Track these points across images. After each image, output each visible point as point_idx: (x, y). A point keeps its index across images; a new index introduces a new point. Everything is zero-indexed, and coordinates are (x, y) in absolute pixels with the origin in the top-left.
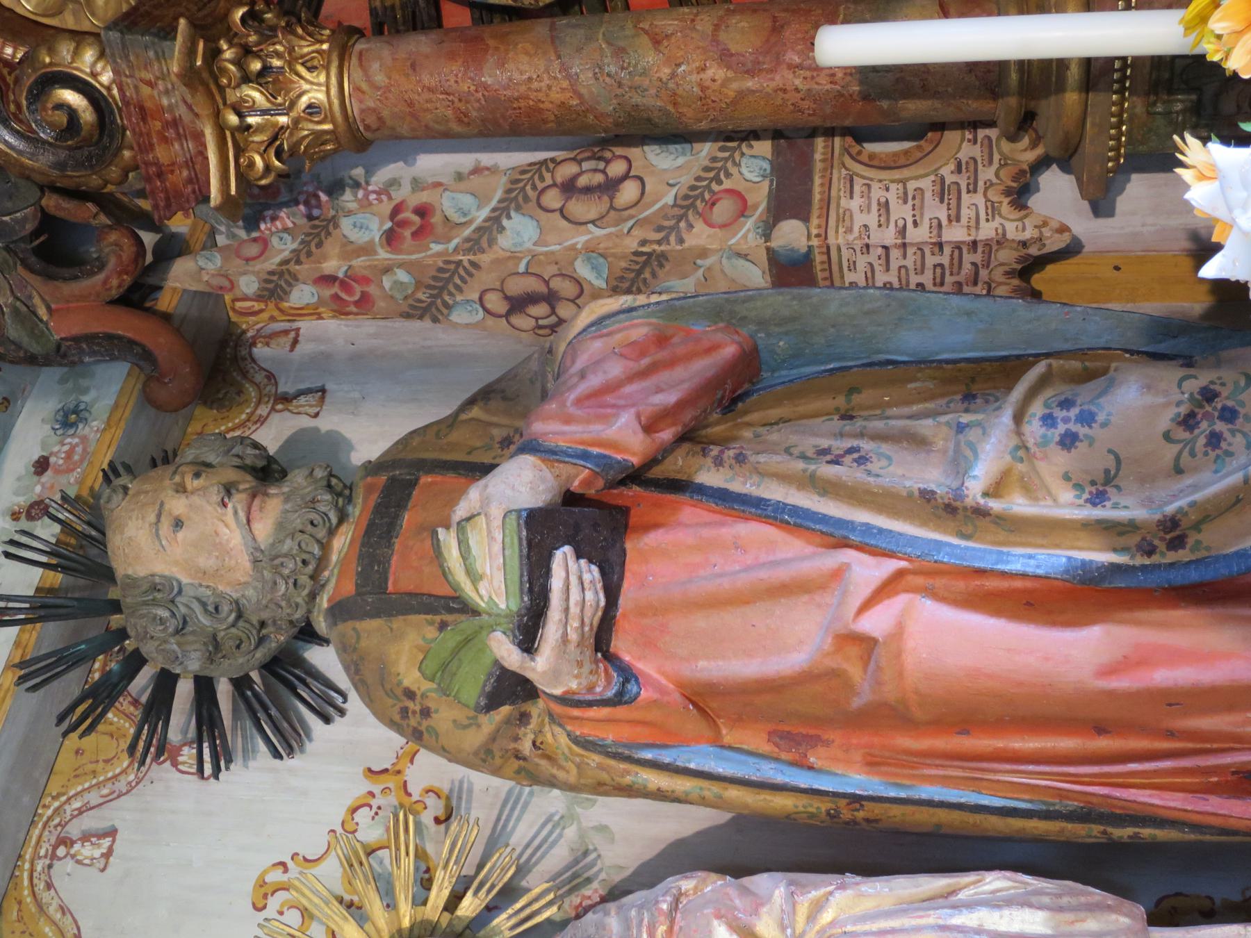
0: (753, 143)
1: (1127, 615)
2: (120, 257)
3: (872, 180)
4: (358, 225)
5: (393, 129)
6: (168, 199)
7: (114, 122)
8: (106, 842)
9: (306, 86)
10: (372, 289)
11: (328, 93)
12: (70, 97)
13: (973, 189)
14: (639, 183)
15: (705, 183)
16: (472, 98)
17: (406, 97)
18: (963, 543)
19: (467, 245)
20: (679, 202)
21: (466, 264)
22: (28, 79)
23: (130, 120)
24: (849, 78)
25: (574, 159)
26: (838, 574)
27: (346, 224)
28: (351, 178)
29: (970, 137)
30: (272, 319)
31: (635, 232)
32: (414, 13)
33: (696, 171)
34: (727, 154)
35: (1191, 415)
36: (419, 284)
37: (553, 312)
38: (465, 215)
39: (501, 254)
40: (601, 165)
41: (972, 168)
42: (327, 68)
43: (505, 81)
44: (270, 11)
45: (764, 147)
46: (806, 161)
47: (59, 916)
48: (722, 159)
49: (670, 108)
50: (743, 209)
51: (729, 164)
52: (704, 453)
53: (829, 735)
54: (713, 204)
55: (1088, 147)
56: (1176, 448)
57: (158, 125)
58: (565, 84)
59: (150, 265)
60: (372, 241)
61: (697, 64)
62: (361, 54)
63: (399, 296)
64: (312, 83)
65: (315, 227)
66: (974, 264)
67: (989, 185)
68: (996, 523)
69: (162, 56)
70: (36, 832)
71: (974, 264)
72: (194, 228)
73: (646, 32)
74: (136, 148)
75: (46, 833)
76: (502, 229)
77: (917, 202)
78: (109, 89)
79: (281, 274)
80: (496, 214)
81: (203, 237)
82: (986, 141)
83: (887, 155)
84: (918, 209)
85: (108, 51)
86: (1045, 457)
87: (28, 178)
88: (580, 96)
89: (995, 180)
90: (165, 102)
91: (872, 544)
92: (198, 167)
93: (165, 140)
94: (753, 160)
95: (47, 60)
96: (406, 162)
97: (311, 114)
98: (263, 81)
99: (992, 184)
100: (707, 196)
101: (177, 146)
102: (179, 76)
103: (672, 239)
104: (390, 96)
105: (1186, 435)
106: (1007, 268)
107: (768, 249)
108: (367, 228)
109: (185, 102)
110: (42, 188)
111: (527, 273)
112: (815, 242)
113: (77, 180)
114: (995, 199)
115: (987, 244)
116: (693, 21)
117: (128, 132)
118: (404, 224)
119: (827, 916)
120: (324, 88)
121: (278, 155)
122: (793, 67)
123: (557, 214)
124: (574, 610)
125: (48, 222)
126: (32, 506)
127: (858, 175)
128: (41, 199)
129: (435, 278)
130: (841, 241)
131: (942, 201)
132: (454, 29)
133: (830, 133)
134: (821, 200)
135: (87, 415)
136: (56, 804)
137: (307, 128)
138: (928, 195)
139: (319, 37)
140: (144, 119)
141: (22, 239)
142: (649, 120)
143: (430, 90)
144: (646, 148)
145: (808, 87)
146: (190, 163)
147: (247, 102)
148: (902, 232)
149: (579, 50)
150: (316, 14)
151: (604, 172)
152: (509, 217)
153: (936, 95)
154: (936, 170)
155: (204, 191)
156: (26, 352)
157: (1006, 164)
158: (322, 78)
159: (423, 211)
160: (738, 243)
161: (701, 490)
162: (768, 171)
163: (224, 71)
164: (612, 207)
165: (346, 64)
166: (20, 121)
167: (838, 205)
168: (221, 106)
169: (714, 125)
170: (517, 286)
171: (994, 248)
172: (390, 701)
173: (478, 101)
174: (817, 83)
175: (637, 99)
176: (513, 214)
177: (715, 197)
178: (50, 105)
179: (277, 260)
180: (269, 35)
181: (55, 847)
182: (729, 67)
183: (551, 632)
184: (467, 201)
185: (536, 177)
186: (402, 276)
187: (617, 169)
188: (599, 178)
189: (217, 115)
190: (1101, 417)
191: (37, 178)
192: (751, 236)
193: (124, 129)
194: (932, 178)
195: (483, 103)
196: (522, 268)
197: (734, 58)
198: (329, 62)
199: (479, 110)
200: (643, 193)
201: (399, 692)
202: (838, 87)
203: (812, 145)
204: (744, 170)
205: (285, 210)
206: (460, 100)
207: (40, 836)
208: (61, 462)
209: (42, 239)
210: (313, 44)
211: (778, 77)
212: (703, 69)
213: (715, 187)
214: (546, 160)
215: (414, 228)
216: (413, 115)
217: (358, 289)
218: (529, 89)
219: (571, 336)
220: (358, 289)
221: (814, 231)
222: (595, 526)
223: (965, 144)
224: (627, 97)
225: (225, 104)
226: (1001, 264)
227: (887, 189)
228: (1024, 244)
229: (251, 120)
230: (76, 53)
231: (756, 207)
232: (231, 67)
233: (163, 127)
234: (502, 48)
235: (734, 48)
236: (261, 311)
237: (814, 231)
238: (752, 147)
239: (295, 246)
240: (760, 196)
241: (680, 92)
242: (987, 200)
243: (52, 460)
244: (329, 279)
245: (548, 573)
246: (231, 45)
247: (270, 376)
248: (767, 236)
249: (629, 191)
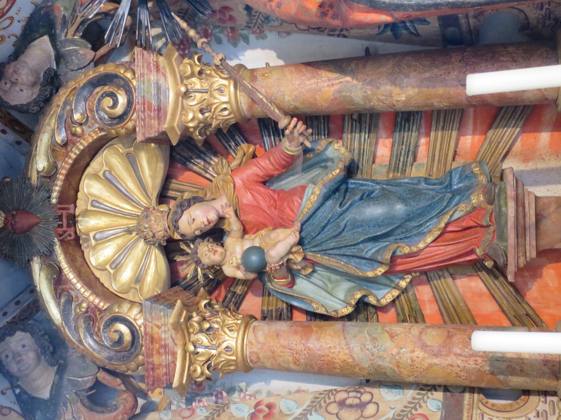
0: (434, 392)
2: (125, 406)
3: (493, 416)
4: (239, 408)
5: (263, 363)
6: (154, 381)
7: (138, 342)
9: (227, 338)
11: (236, 342)
12: (123, 328)
14: (376, 406)
15: (409, 409)
16: (302, 353)
17: (272, 349)
20: (396, 417)
23: (146, 342)
24: (484, 363)
25: (346, 391)
27: (233, 408)
28: (239, 387)
29: (543, 400)
32: (281, 314)
33: (405, 403)
34: (420, 397)
38: (290, 411)
40: (359, 395)
41: (545, 415)
42: (238, 331)
43: (318, 347)
44: (217, 304)
45: (439, 395)
46: (459, 404)
48: (418, 399)
49: (396, 369)
51: (421, 402)
57: (157, 346)
58: (347, 351)
59: (138, 414)
61: (411, 349)
62: (254, 327)
65: (218, 407)
69: (166, 316)
72: (162, 400)
73: (387, 332)
74: (145, 355)
78: (140, 327)
80: (305, 412)
81: (165, 405)
82: (551, 403)
83: (501, 405)
85: (144, 310)
87: (94, 362)
88: (353, 358)
90: (163, 336)
92: (171, 368)
93: (159, 353)
94: (433, 401)
95: (117, 310)
96: (266, 383)
97: (227, 351)
98: (208, 333)
100: (409, 416)
101: (164, 357)
102: (172, 324)
104: (265, 347)
108: (243, 411)
109: (172, 337)
110: (99, 368)
113: (115, 366)
116: (410, 329)
117: (143, 348)
118: (260, 411)
120: (235, 340)
121: (208, 368)
122: (457, 355)
123: (335, 415)
125: (97, 384)
127: (486, 413)
128: (97, 373)
132: (298, 322)
133: (472, 390)
137: (224, 357)
139: (237, 317)
140: (152, 342)
141: (83, 390)
142: (385, 373)
143: (284, 347)
144: (381, 389)
145: (463, 365)
146: (168, 366)
147: (200, 341)
149: (355, 336)
150: (238, 309)
151: (359, 398)
152: (311, 414)
153: (527, 375)
154: (526, 415)
155: (171, 381)
158: (235, 335)
159: (270, 406)
162: (441, 407)
163: (192, 326)
164: (362, 416)
165: (247, 331)
166: (98, 336)
168: (187, 342)
169: (416, 379)
173: (305, 355)
174: (469, 364)
175: (380, 363)
176: (313, 413)
177: (414, 417)
178: (113, 330)
180: (215, 313)
182: (426, 352)
184: (292, 404)
185: (327, 397)
187: (366, 398)
188: (357, 401)
189: (185, 345)
191: (98, 363)
193: (142, 346)
195: (307, 356)
197: (428, 348)
198: (239, 329)
199: (305, 359)
200: (378, 411)
202: (478, 367)
203: (463, 396)
204: (428, 405)
205: (206, 398)
206: (297, 353)
209: (93, 392)
210: (234, 320)
211: (449, 359)
212: (413, 352)
213: (414, 412)
214: (332, 390)
215: (265, 414)
216: (273, 358)
218: (330, 352)
223: (541, 403)
224: (375, 361)
225: (189, 341)
229: (200, 350)
230: (130, 309)
232: (196, 325)
233: (159, 347)
234: (319, 332)
235: (429, 343)
238: (433, 394)
239: (207, 414)
241: (401, 361)
246: (198, 315)
249: (371, 409)
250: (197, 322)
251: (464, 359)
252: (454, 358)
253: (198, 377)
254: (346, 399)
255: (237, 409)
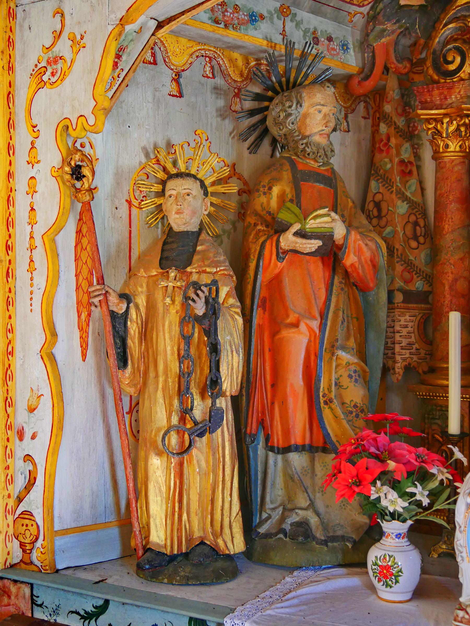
1: (306, 391)
8: (211, 75)
10: (384, 154)
12: (458, 60)
13: (411, 353)
18: (324, 350)
19: (398, 190)
20: (410, 261)
21: (392, 189)
22: (464, 47)
26: (314, 318)
30: (372, 108)
31: (401, 247)
33: (420, 266)
34: (424, 276)
35: (357, 407)
36: (386, 171)
37: (374, 217)
39: (395, 202)
47: (189, 62)
49: (441, 262)
50: (407, 282)
51: (421, 277)
52: (343, 279)
53: (267, 314)
54: (409, 272)
55: (423, 387)
56: (349, 403)
57: (446, 93)
60: (401, 155)
63: (382, 163)
64: (456, 146)
66: (388, 354)
67: (412, 358)
68: (329, 358)
70: (212, 49)
71: (388, 354)
73: (464, 256)
75: (212, 53)
76: (403, 201)
77: (407, 337)
79: (391, 122)
84: (405, 337)
86: (346, 370)
88: (446, 235)
89: (413, 360)
91: (322, 327)
93: (441, 94)
99: (412, 359)
100: (411, 270)
101: (438, 98)
103: (398, 259)
105: (352, 406)
106: (386, 363)
107: (394, 290)
108: (405, 153)
111: (388, 210)
112: (396, 305)
114: (408, 360)
115: (394, 358)
118: (406, 166)
119: (237, 317)
123: (407, 220)
124: (305, 246)
126: (317, 38)
129: (388, 177)
130: (396, 313)
131: (407, 344)
134: (409, 307)
135: (346, 53)
136: (221, 55)
138: (409, 340)
148: (398, 332)
151: (421, 235)
152: (407, 204)
156: (370, 33)
157: (418, 364)
160: (396, 280)
161: (333, 278)
164: (409, 239)
167: (407, 312)
170: (384, 206)
171: (393, 360)
172: (267, 182)
173: (447, 201)
175: (444, 253)
176: (408, 205)
179: (396, 120)
181: (208, 57)
182: (452, 281)
183: (300, 240)
184: (413, 188)
185: (420, 212)
186: (389, 166)
187: (422, 240)
188: (419, 234)
190: (356, 384)
192: (398, 285)
194: (415, 341)
196: (390, 208)
201: (270, 185)
204: (419, 282)
207: (211, 51)
208: (331, 46)
211: (448, 296)
212: (452, 273)
213: (414, 273)
215: (405, 170)
217: (385, 149)
219: (376, 238)
220: (385, 149)
221: (399, 305)
222: (326, 250)
223: (425, 351)
226: (387, 362)
227: (411, 327)
228: (394, 369)
231: (408, 286)
232: (463, 122)
235: (458, 283)
236: (375, 104)
237: (399, 305)
239: (401, 127)
240: (410, 287)
241: (446, 266)
242: (407, 358)
243: (332, 43)
244: (388, 139)
245: (315, 239)
247: (353, 110)
248: (398, 290)
249: (414, 244)
250: (465, 122)
251: (449, 305)
252: (449, 299)
253: (426, 126)
254: (419, 226)
255: (407, 148)
